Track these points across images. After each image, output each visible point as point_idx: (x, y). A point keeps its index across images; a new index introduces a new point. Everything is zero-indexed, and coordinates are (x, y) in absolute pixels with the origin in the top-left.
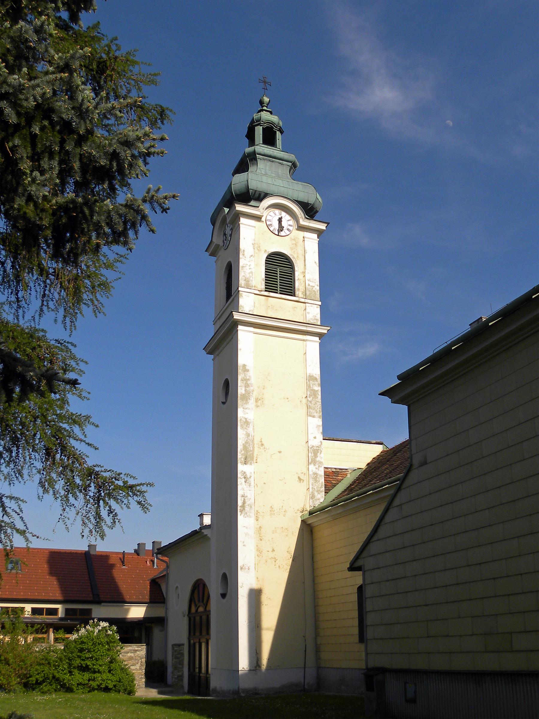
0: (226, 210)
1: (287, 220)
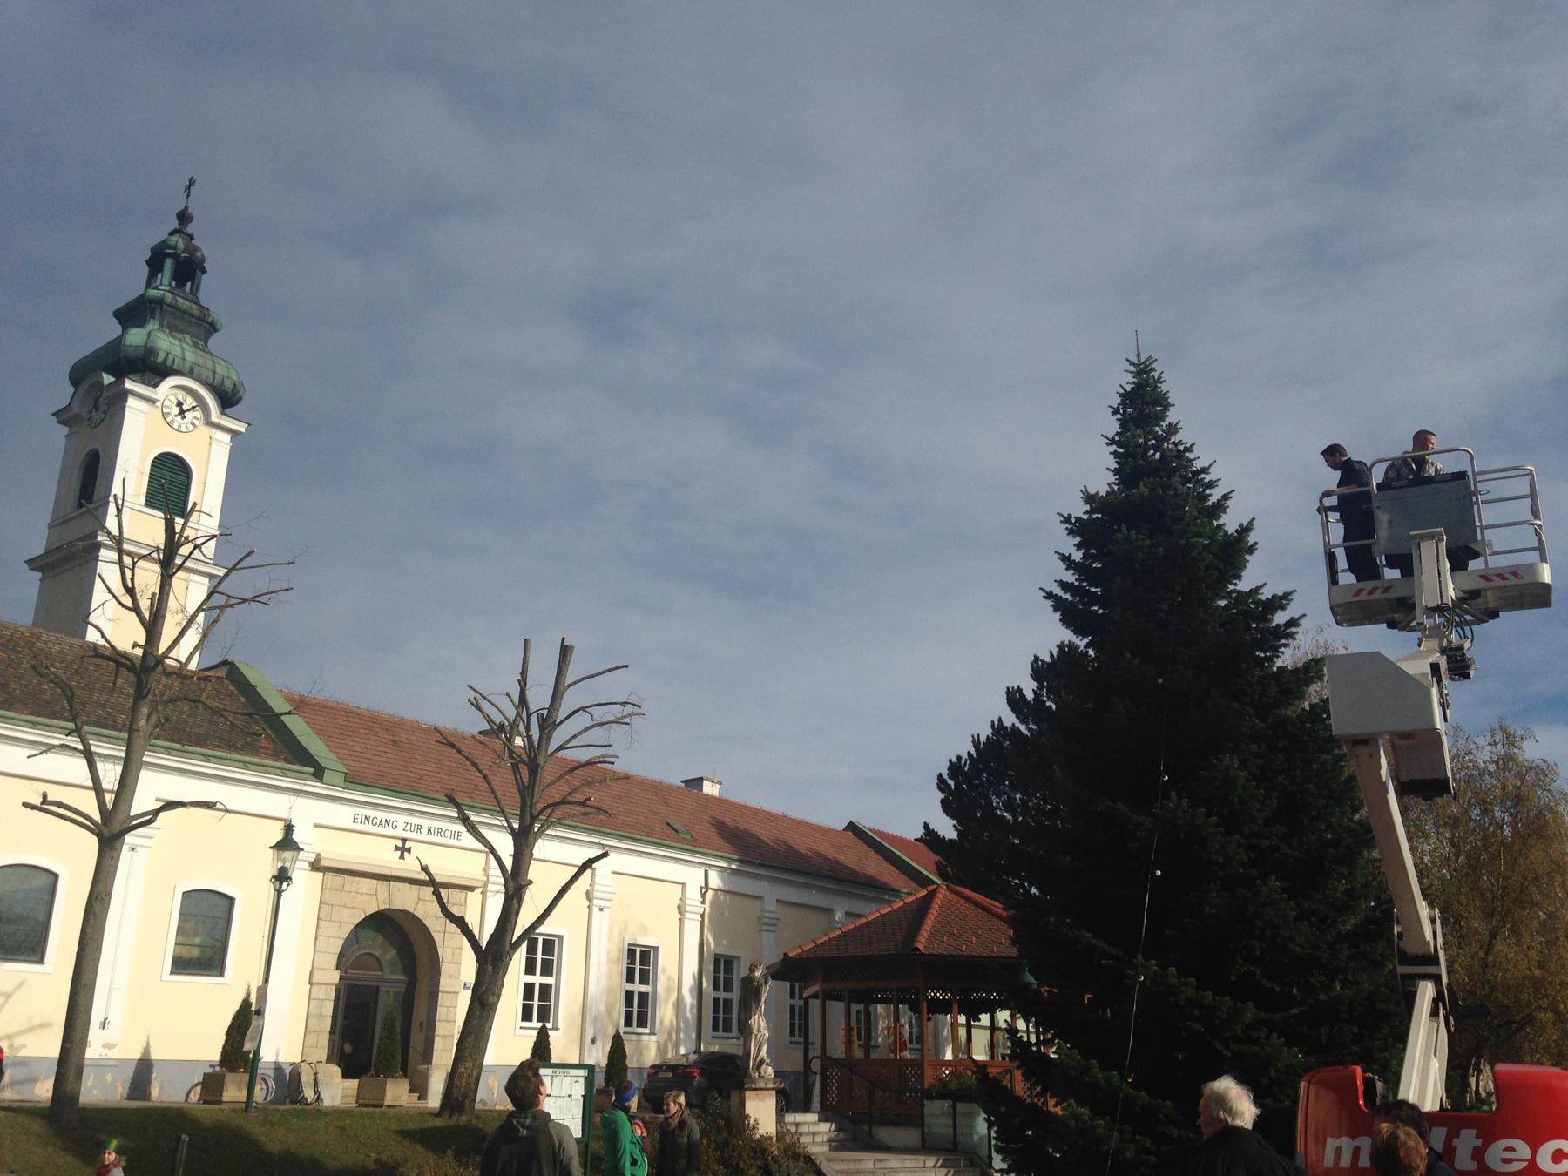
1: (189, 402)
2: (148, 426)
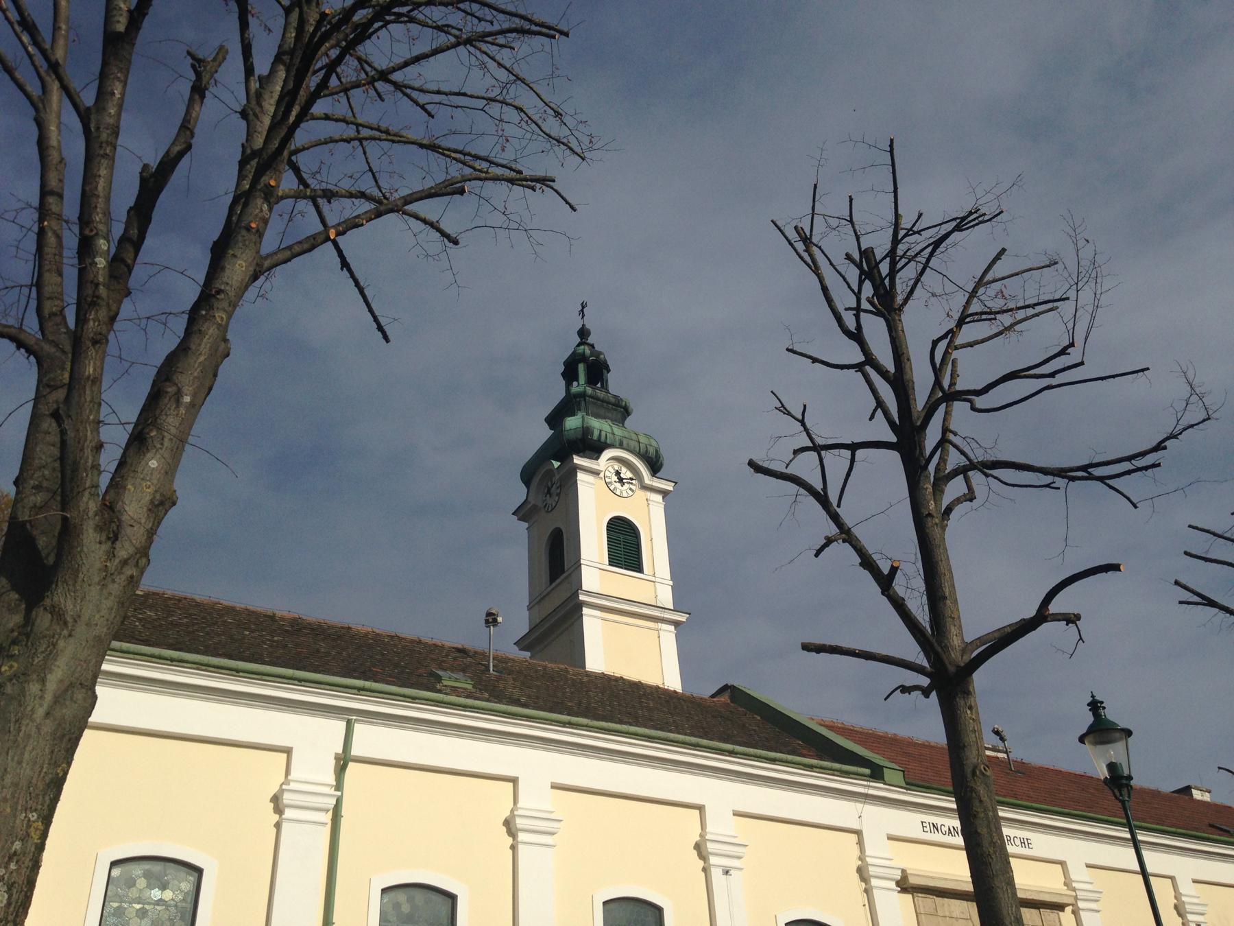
0: (556, 464)
1: (626, 474)
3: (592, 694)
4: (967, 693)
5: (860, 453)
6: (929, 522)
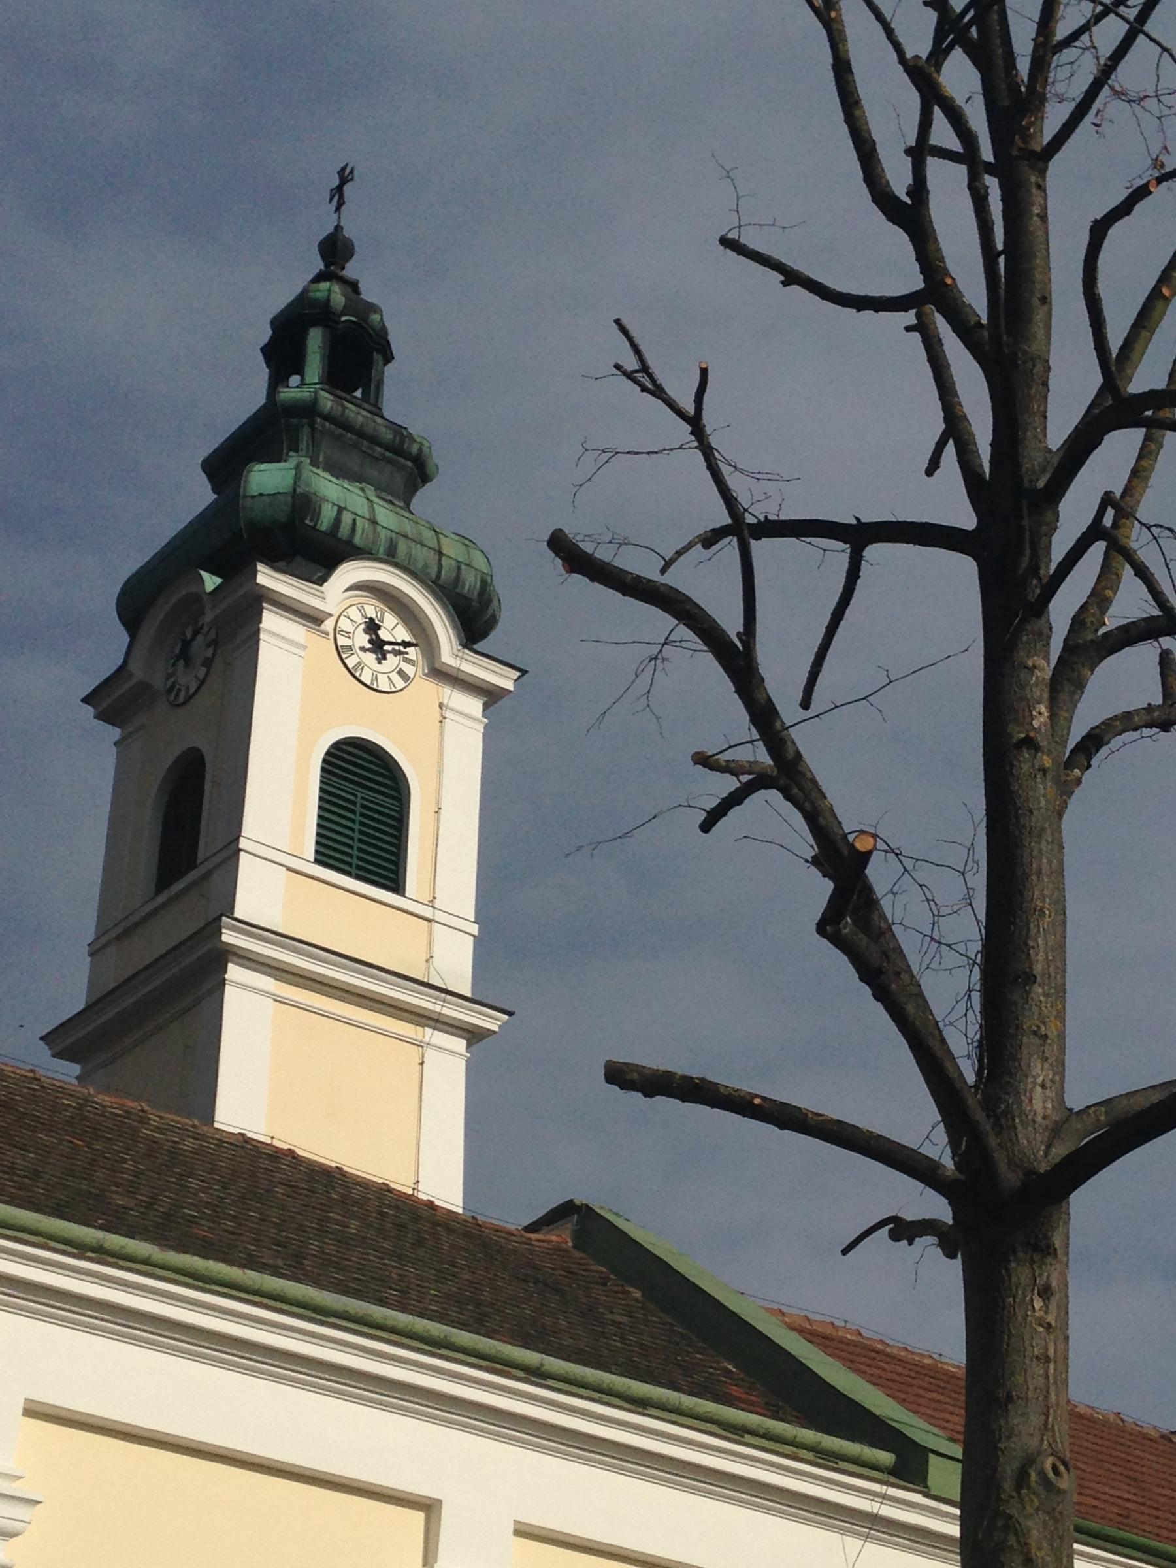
0: (211, 582)
1: (393, 629)
2: (313, 678)
3: (194, 1184)
4: (1043, 1249)
5: (874, 552)
6: (1024, 763)
